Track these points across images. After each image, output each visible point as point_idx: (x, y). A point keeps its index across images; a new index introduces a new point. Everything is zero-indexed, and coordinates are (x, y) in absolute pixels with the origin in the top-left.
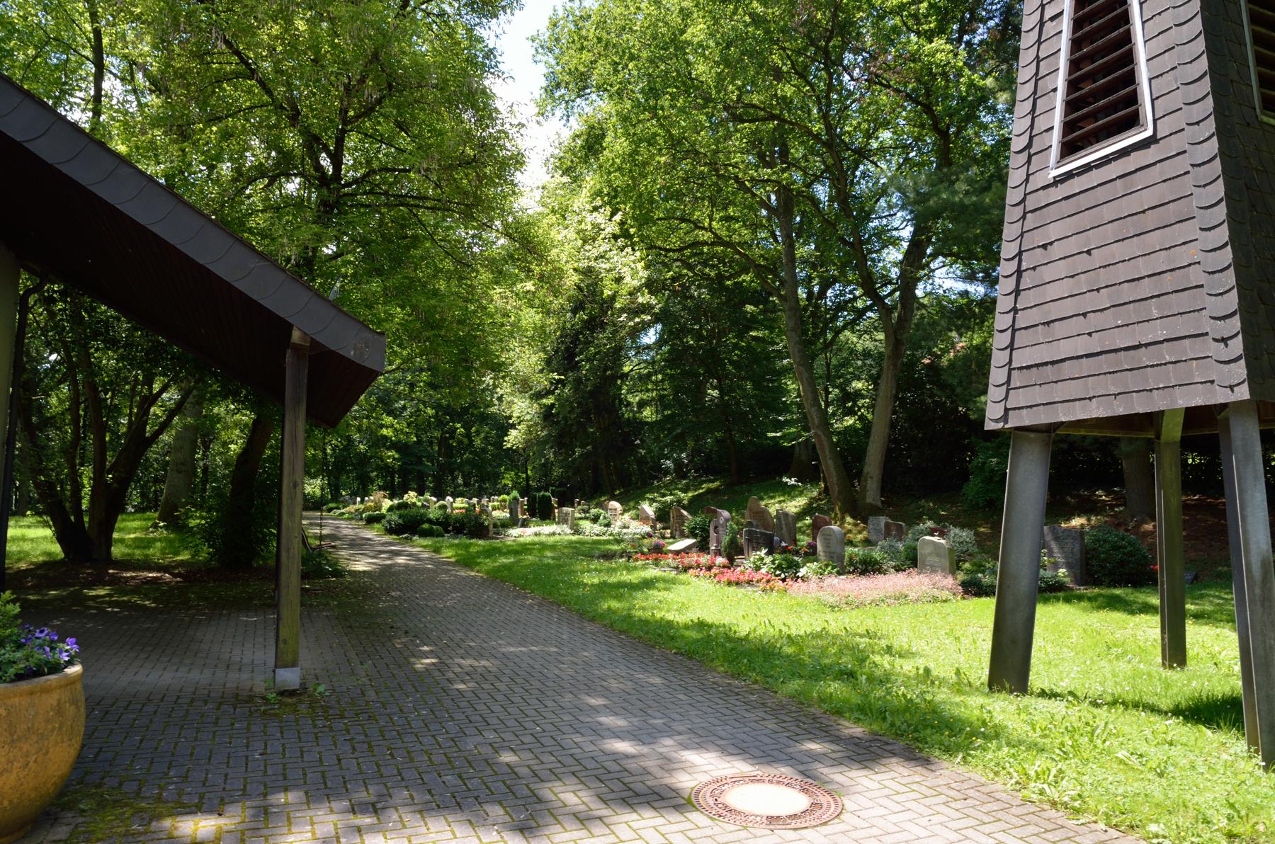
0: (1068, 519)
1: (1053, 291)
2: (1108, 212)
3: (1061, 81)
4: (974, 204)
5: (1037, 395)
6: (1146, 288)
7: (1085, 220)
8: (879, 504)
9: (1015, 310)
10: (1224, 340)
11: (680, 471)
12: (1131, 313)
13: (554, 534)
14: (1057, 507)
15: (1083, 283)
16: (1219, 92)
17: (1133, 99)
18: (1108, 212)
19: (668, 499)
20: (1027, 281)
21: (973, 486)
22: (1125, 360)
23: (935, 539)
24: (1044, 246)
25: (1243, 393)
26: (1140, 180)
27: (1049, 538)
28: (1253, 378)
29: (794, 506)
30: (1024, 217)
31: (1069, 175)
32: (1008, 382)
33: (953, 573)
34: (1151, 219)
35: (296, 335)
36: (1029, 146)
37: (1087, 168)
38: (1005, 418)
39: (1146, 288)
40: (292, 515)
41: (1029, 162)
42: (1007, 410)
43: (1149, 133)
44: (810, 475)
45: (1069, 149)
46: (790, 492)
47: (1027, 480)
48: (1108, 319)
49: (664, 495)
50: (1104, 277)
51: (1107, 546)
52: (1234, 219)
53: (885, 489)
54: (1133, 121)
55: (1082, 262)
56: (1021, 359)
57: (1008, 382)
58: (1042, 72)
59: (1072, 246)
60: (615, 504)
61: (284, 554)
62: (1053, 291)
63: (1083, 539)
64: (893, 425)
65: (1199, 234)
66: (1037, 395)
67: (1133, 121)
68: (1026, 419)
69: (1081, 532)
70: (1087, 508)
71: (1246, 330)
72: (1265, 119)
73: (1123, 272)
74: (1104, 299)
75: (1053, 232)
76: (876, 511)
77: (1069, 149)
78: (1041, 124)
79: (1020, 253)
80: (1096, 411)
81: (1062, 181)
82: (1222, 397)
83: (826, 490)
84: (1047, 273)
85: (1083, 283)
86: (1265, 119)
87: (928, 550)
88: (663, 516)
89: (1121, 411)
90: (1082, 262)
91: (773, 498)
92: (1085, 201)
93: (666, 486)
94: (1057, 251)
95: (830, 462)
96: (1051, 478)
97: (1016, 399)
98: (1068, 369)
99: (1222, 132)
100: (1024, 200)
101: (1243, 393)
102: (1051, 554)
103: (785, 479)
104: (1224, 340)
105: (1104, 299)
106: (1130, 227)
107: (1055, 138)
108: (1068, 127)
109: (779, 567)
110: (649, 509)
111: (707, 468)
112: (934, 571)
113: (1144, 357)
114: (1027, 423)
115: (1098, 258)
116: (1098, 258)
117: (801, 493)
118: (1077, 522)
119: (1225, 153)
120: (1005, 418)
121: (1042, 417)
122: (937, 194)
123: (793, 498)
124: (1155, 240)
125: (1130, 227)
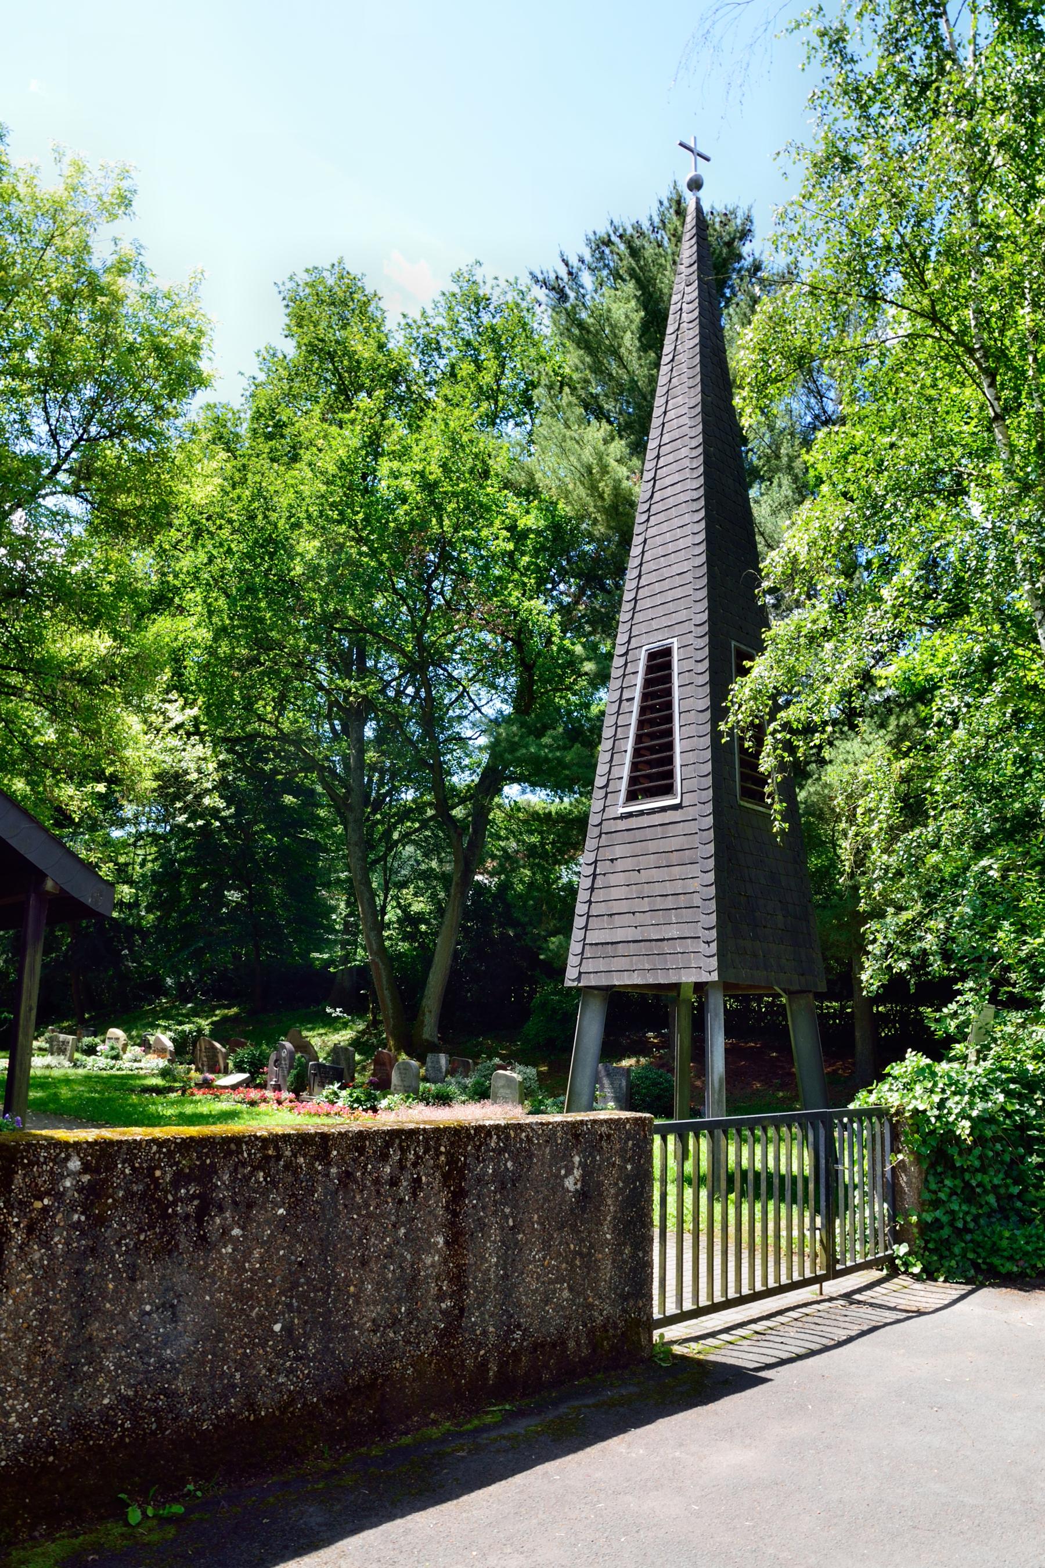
0: (620, 1060)
1: (615, 893)
2: (652, 847)
3: (630, 745)
4: (557, 758)
5: (601, 965)
6: (669, 903)
7: (638, 848)
8: (436, 1040)
9: (590, 902)
10: (708, 943)
11: (184, 994)
12: (660, 917)
13: (48, 1067)
14: (610, 1051)
15: (634, 891)
16: (716, 786)
17: (670, 775)
18: (652, 847)
19: (187, 1027)
20: (599, 883)
21: (532, 1026)
22: (655, 948)
23: (508, 1073)
24: (612, 860)
25: (715, 977)
26: (672, 830)
27: (603, 1073)
28: (720, 969)
29: (344, 1037)
30: (600, 836)
31: (630, 815)
32: (582, 953)
33: (521, 1103)
34: (675, 858)
35: (49, 885)
36: (606, 786)
37: (641, 813)
38: (578, 979)
39: (669, 903)
40: (26, 1035)
41: (606, 797)
42: (580, 973)
43: (677, 801)
44: (356, 1007)
45: (632, 796)
46: (332, 1024)
47: (590, 1028)
48: (647, 919)
49: (181, 1023)
50: (647, 890)
51: (648, 1082)
52: (718, 869)
53: (444, 1024)
54: (668, 790)
55: (634, 877)
56: (593, 937)
57: (582, 953)
58: (619, 736)
59: (628, 864)
60: (116, 1032)
61: (17, 1068)
62: (615, 893)
63: (629, 1076)
64: (456, 954)
65: (699, 874)
66: (601, 965)
67: (668, 790)
68: (592, 981)
69: (628, 1070)
70: (639, 1049)
71: (719, 938)
72: (742, 803)
73: (658, 889)
74: (645, 904)
75: (618, 851)
76: (435, 1049)
77: (632, 796)
78: (615, 773)
79: (596, 862)
80: (636, 979)
81: (626, 818)
82: (705, 978)
83: (375, 1023)
84: (613, 879)
85: (634, 891)
86: (742, 803)
87: (501, 1083)
88: (183, 1048)
89: (651, 981)
90: (634, 877)
91: (312, 1029)
92: (639, 835)
93: (186, 1016)
94: (620, 865)
95: (386, 992)
96: (607, 1019)
97: (589, 966)
98: (621, 949)
99: (717, 813)
100: (600, 824)
101: (715, 977)
102: (602, 1087)
103: (328, 1010)
104: (708, 943)
105: (645, 904)
106: (663, 860)
107: (624, 785)
108: (633, 781)
109: (358, 1100)
110: (166, 1039)
111: (217, 990)
112: (506, 1100)
113: (666, 947)
114: (593, 984)
115: (644, 876)
116: (644, 876)
117: (345, 1025)
118: (625, 1063)
119: (717, 826)
120: (578, 979)
121: (603, 981)
122: (526, 746)
123: (337, 1030)
124: (676, 871)
125: (663, 860)
